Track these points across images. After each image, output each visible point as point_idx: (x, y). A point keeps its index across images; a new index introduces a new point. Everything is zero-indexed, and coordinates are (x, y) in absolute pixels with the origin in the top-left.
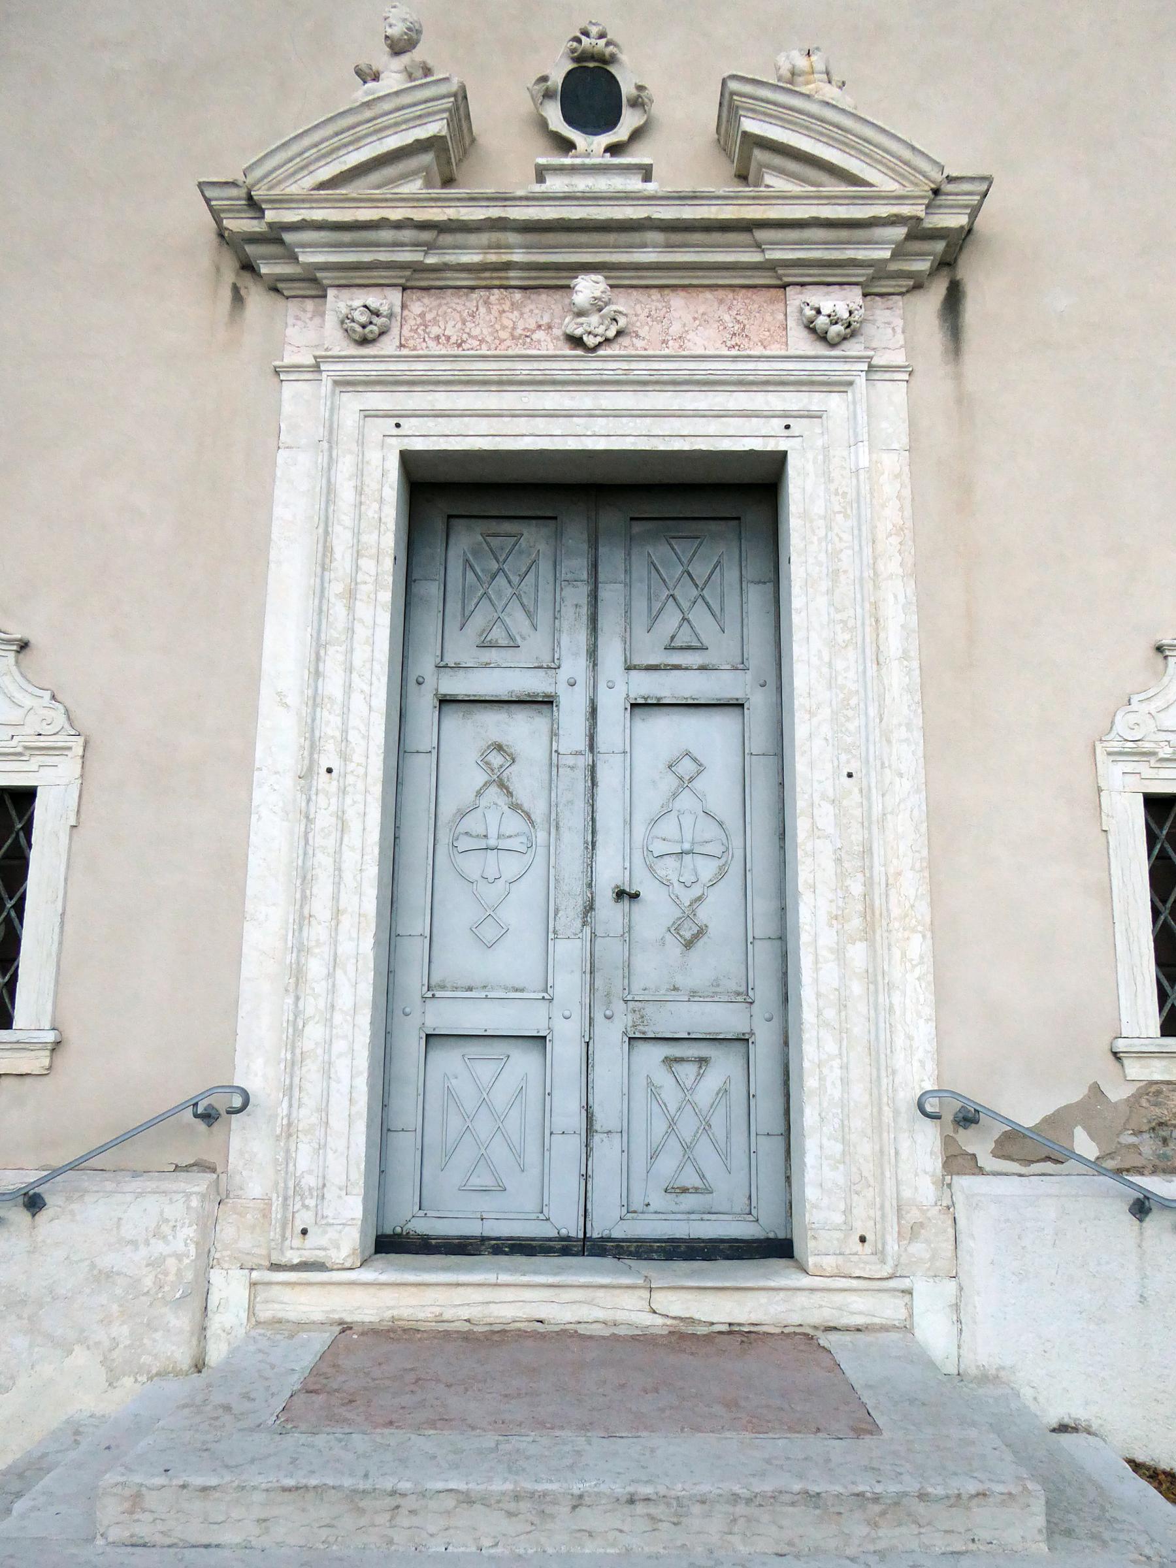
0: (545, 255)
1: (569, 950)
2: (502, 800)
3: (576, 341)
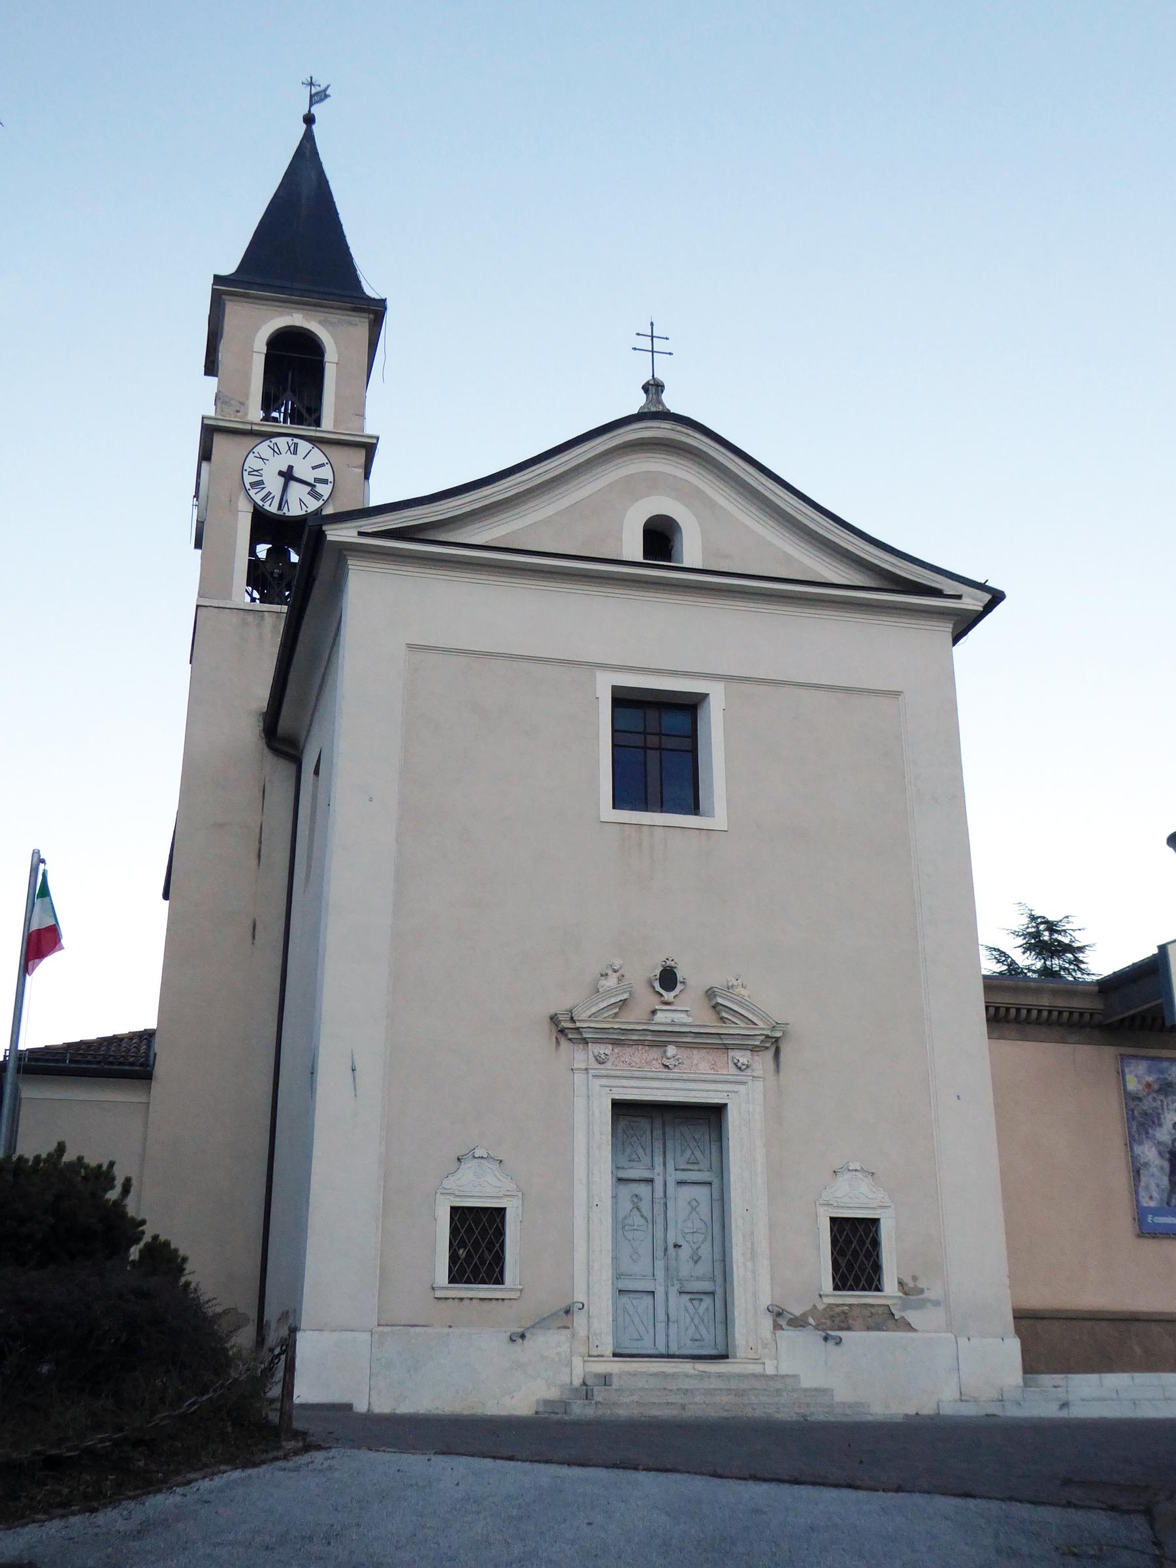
0: (659, 1040)
1: (660, 1264)
2: (638, 1214)
3: (666, 1066)
